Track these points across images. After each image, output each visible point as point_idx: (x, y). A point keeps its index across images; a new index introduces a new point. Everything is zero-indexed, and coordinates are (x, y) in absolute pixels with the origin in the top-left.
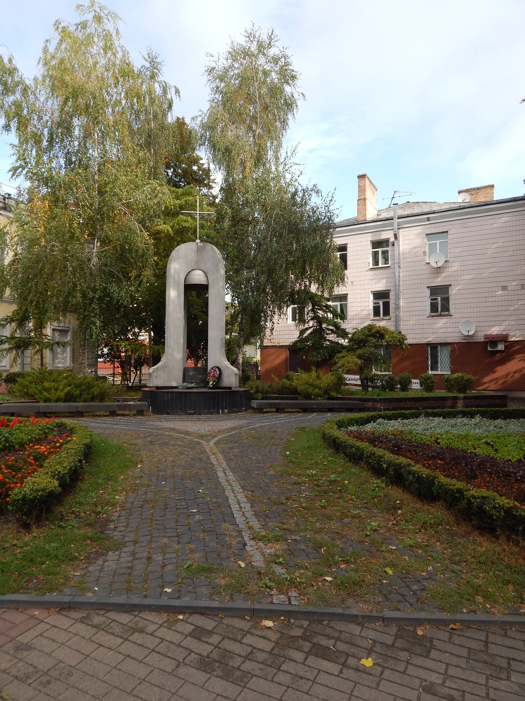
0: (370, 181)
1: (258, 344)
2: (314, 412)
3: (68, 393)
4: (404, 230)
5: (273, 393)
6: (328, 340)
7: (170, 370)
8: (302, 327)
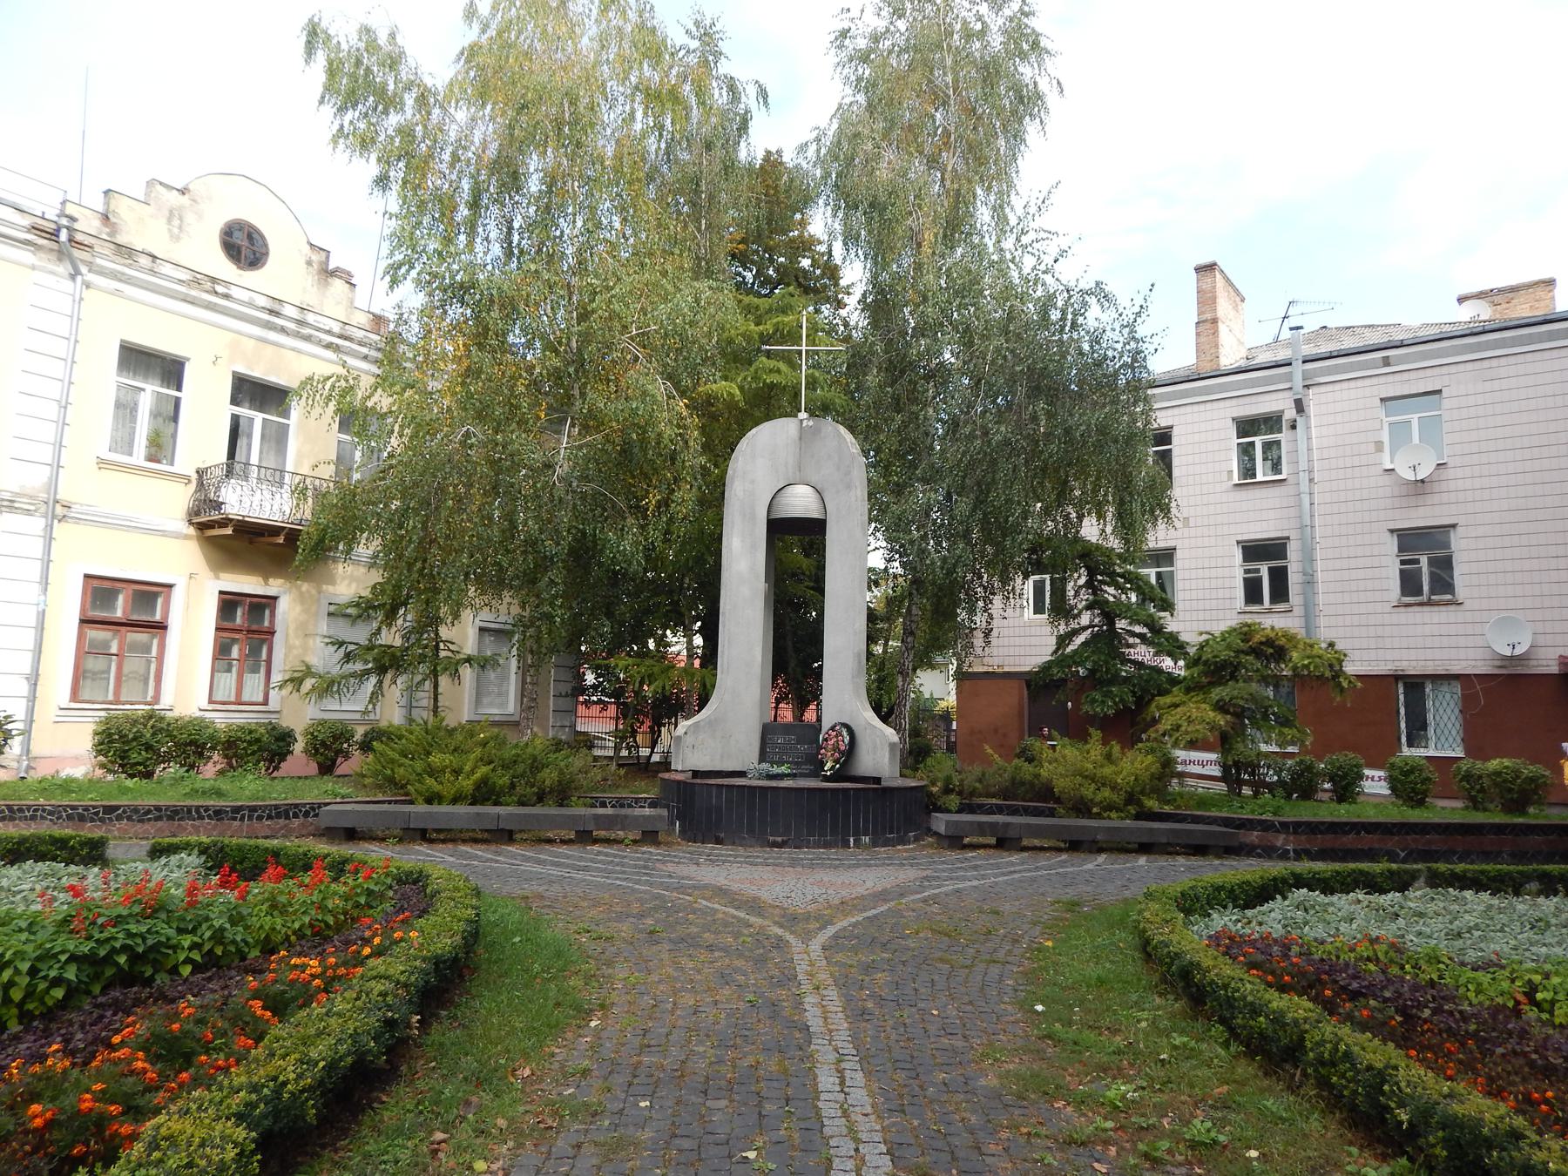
0: (1228, 280)
1: (952, 668)
2: (1100, 850)
3: (484, 781)
4: (1323, 389)
5: (989, 795)
6: (1131, 661)
7: (723, 734)
8: (1062, 629)
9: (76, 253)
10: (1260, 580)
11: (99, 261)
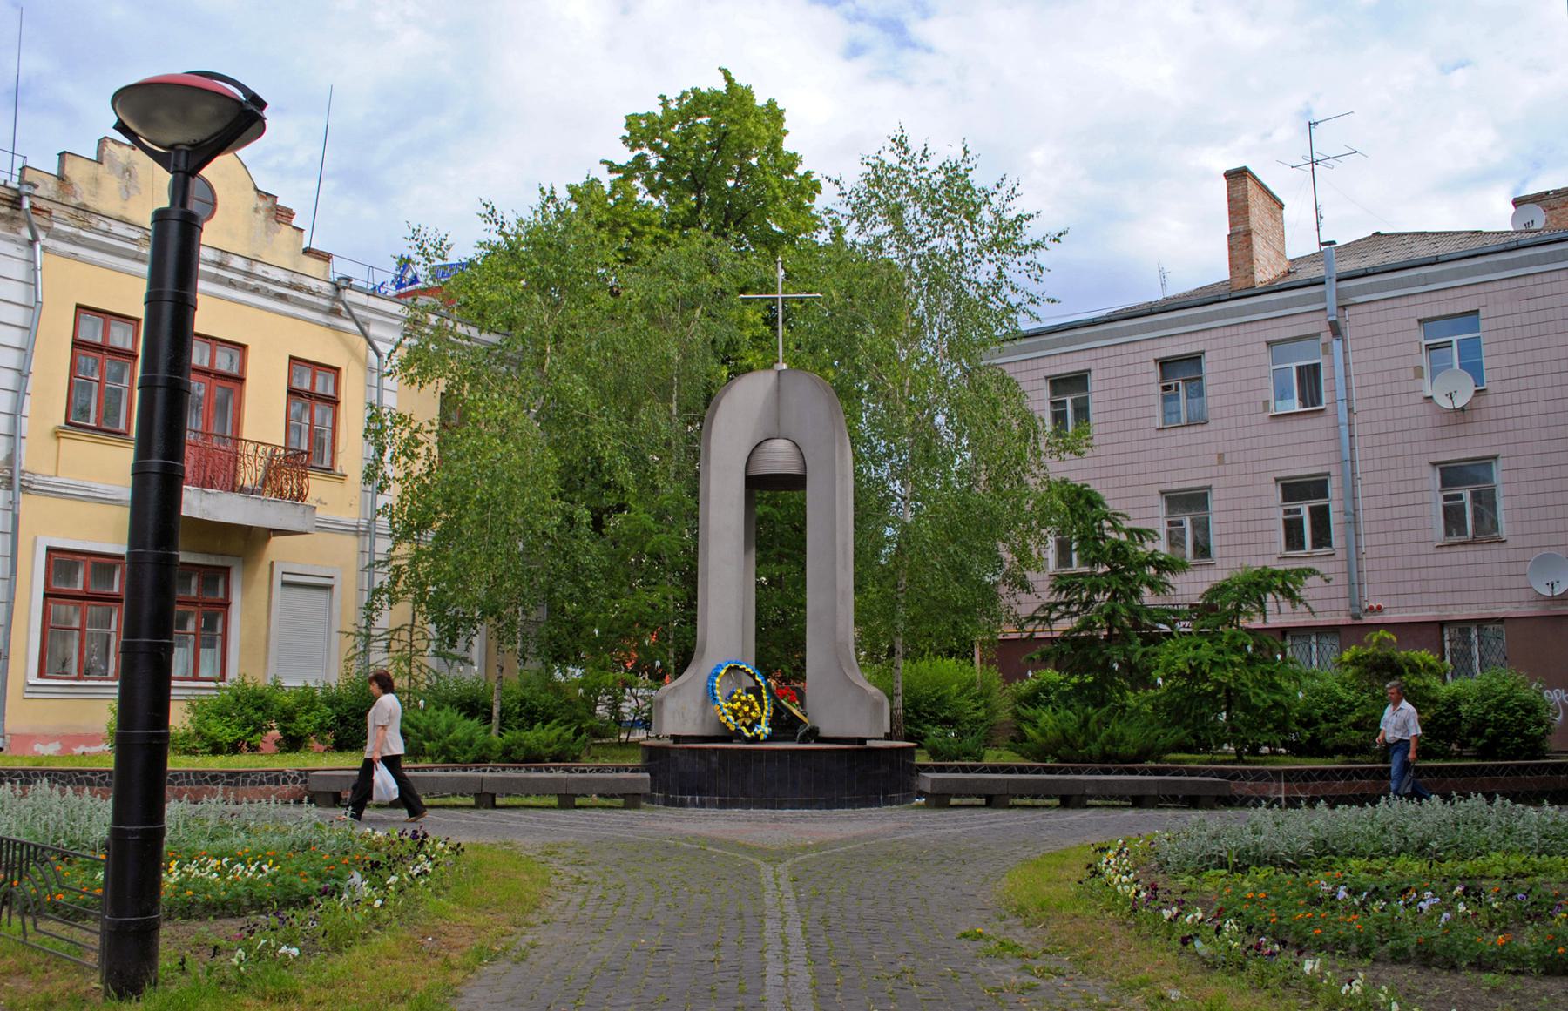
9: (36, 219)
10: (1301, 521)
11: (56, 225)
